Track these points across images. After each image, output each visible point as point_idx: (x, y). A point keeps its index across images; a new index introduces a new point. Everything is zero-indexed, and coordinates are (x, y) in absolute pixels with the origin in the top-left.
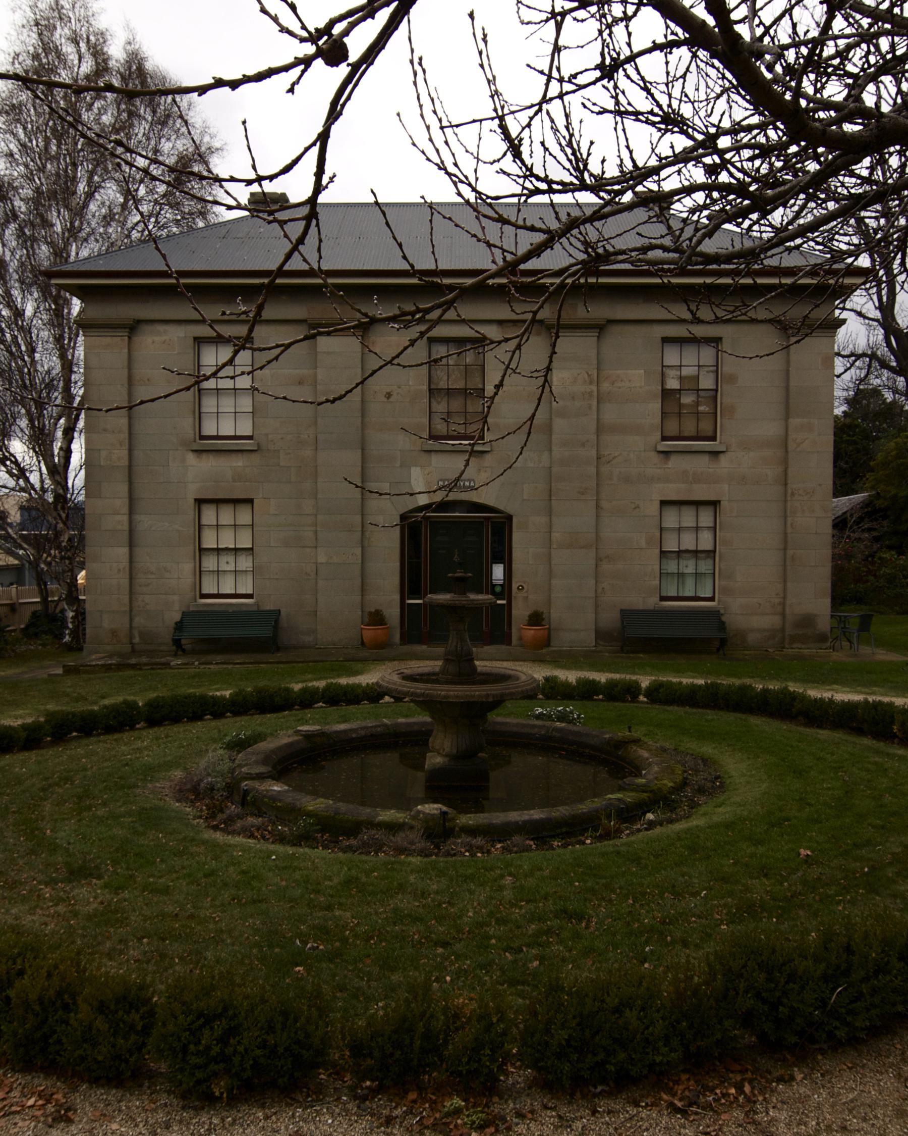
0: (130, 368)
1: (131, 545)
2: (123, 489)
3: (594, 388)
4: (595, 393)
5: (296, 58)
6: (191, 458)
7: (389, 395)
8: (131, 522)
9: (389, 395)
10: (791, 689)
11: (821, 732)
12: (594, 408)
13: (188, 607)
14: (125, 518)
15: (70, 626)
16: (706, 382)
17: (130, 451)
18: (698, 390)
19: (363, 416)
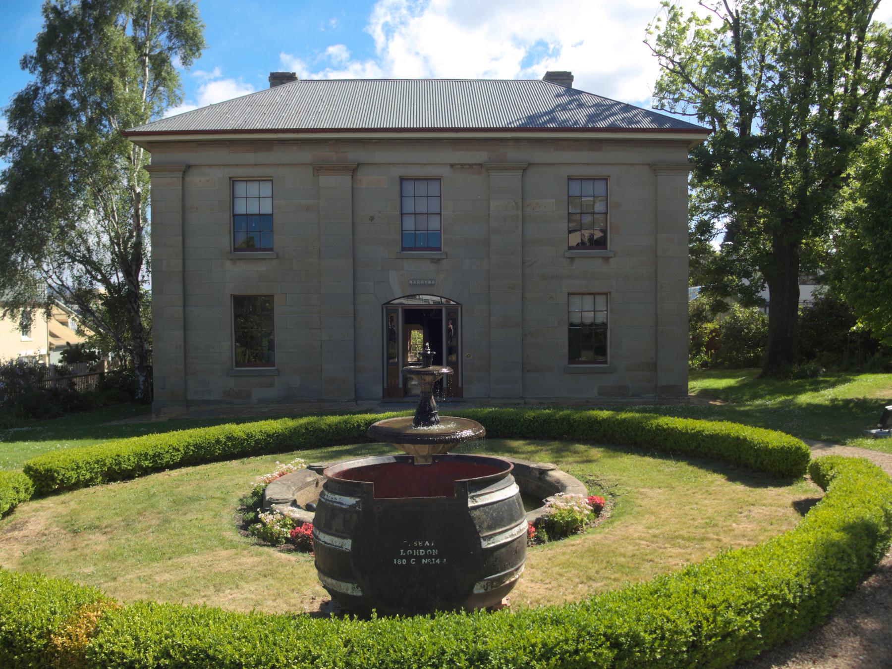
0: (183, 201)
1: (185, 328)
2: (179, 288)
3: (520, 213)
4: (521, 216)
5: (68, 343)
6: (228, 264)
7: (372, 218)
8: (184, 311)
9: (372, 218)
10: (350, 586)
11: (809, 401)
12: (520, 227)
13: (518, 75)
14: (181, 309)
15: (142, 387)
16: (599, 207)
17: (184, 260)
18: (594, 213)
19: (353, 234)
